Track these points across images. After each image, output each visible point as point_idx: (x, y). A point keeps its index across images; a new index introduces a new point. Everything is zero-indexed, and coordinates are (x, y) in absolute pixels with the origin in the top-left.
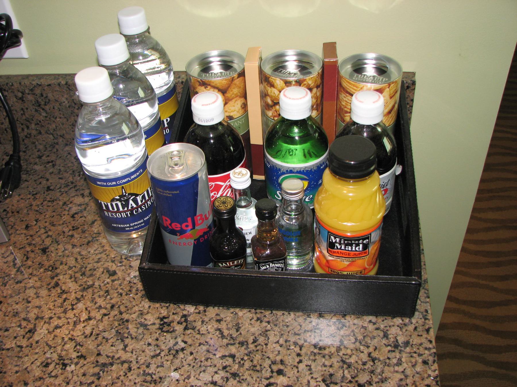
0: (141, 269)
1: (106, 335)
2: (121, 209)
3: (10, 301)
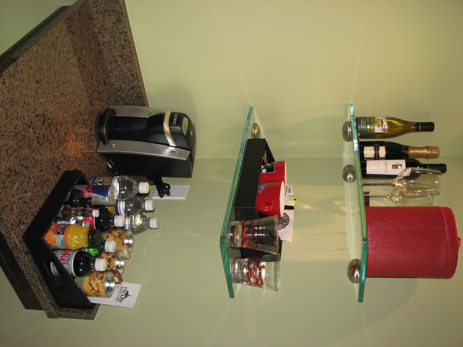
0: (81, 171)
1: (65, 151)
2: (99, 181)
3: (84, 136)
